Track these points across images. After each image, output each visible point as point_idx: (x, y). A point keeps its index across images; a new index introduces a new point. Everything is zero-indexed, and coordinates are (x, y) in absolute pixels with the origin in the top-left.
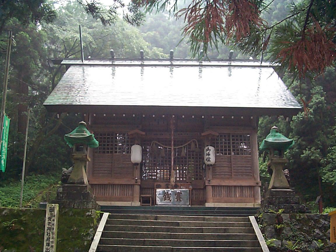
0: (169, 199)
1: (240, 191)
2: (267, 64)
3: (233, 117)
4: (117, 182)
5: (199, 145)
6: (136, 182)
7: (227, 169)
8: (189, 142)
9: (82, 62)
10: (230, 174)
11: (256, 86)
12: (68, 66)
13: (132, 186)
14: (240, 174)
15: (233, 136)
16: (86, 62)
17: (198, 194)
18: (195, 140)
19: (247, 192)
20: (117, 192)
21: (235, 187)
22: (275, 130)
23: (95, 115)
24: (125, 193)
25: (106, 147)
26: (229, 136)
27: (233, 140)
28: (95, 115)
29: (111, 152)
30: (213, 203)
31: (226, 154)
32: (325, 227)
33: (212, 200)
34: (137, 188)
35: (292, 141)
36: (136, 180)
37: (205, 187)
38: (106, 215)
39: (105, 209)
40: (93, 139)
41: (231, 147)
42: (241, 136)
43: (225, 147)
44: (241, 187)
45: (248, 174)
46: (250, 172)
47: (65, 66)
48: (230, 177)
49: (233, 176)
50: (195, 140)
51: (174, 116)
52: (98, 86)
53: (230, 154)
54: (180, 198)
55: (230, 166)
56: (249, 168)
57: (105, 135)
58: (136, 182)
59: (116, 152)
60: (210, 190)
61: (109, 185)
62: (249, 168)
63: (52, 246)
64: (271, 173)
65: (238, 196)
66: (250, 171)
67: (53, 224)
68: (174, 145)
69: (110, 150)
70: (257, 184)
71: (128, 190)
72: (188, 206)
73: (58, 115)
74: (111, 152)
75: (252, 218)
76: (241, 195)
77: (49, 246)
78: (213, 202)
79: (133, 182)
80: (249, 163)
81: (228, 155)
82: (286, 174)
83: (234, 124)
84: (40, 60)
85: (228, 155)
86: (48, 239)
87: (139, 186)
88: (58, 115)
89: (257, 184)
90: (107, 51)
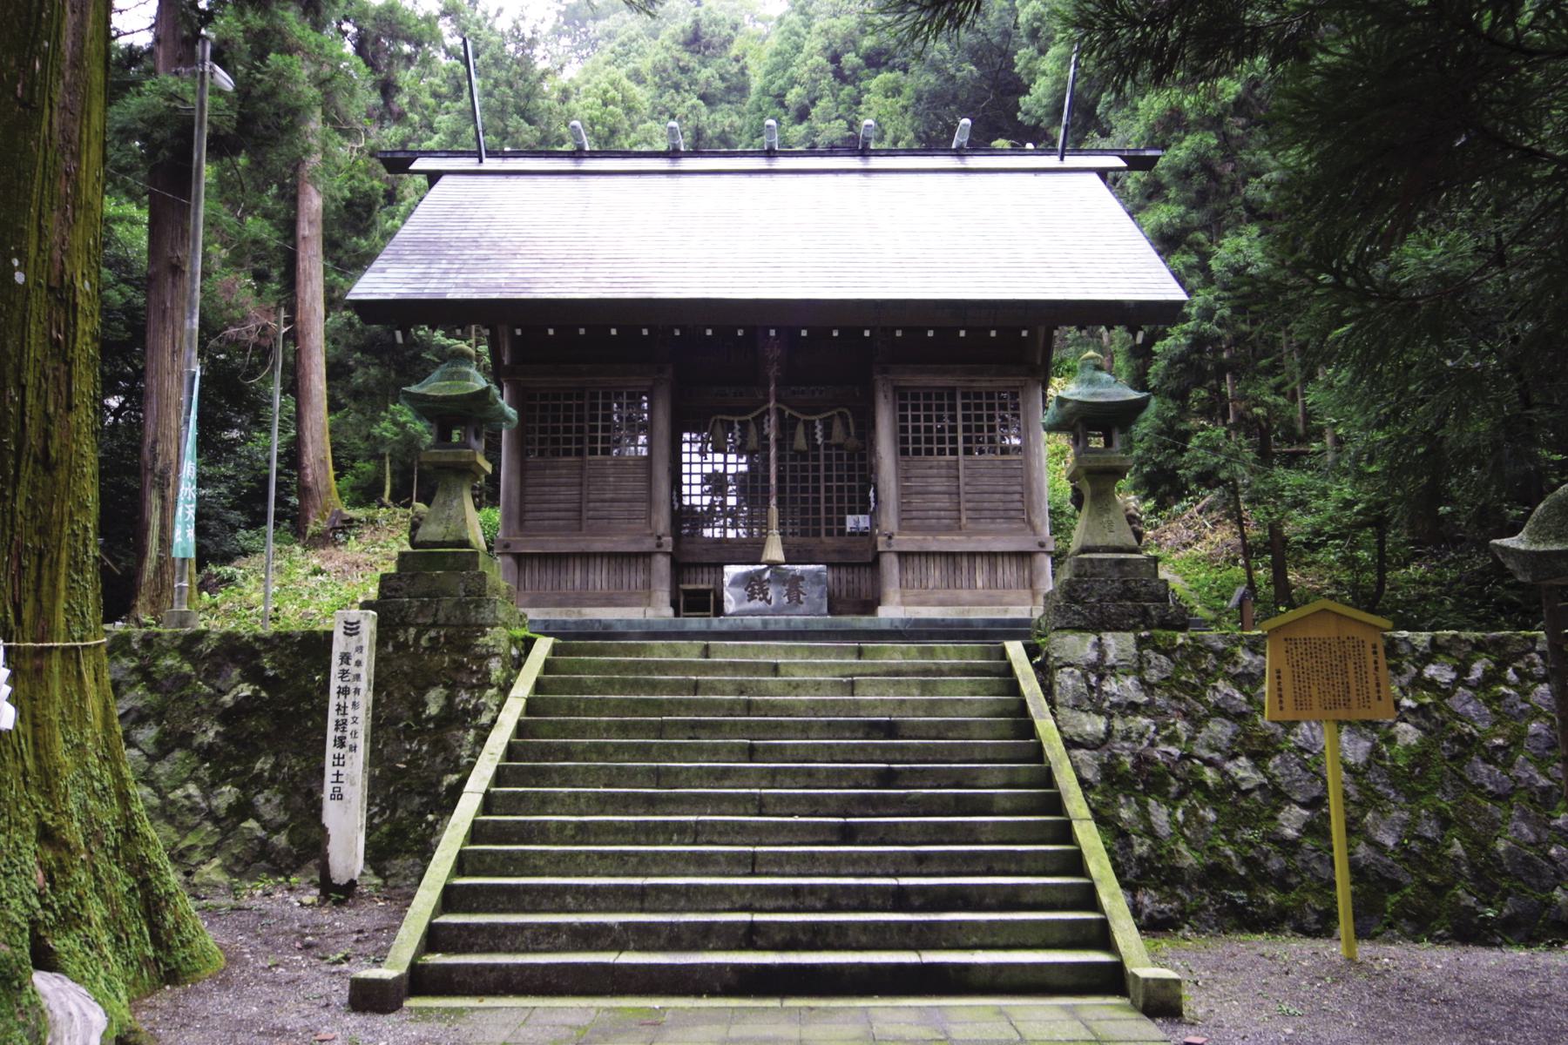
1: (986, 567)
3: (993, 333)
4: (599, 545)
5: (857, 428)
6: (659, 545)
7: (944, 501)
10: (954, 514)
11: (1052, 232)
12: (433, 177)
13: (648, 555)
14: (987, 514)
15: (965, 396)
19: (1008, 572)
20: (600, 578)
21: (972, 555)
23: (519, 332)
24: (625, 580)
25: (561, 435)
26: (952, 397)
28: (519, 332)
29: (580, 453)
31: (941, 452)
32: (1250, 675)
33: (897, 598)
34: (662, 565)
37: (877, 556)
41: (960, 430)
42: (990, 395)
44: (992, 556)
45: (1013, 513)
46: (1019, 509)
48: (955, 528)
49: (964, 521)
51: (773, 333)
52: (511, 235)
53: (954, 452)
55: (954, 489)
56: (1017, 497)
57: (568, 397)
58: (659, 545)
59: (593, 452)
60: (891, 566)
61: (574, 555)
62: (1017, 497)
63: (353, 748)
64: (1079, 506)
65: (979, 584)
66: (1019, 505)
67: (358, 677)
70: (1042, 545)
73: (399, 334)
74: (580, 453)
75: (1015, 649)
76: (992, 583)
77: (342, 745)
79: (648, 545)
80: (1013, 481)
81: (948, 457)
83: (981, 352)
84: (1173, 122)
85: (599, 457)
86: (341, 725)
88: (399, 334)
89: (1042, 545)
90: (521, 126)
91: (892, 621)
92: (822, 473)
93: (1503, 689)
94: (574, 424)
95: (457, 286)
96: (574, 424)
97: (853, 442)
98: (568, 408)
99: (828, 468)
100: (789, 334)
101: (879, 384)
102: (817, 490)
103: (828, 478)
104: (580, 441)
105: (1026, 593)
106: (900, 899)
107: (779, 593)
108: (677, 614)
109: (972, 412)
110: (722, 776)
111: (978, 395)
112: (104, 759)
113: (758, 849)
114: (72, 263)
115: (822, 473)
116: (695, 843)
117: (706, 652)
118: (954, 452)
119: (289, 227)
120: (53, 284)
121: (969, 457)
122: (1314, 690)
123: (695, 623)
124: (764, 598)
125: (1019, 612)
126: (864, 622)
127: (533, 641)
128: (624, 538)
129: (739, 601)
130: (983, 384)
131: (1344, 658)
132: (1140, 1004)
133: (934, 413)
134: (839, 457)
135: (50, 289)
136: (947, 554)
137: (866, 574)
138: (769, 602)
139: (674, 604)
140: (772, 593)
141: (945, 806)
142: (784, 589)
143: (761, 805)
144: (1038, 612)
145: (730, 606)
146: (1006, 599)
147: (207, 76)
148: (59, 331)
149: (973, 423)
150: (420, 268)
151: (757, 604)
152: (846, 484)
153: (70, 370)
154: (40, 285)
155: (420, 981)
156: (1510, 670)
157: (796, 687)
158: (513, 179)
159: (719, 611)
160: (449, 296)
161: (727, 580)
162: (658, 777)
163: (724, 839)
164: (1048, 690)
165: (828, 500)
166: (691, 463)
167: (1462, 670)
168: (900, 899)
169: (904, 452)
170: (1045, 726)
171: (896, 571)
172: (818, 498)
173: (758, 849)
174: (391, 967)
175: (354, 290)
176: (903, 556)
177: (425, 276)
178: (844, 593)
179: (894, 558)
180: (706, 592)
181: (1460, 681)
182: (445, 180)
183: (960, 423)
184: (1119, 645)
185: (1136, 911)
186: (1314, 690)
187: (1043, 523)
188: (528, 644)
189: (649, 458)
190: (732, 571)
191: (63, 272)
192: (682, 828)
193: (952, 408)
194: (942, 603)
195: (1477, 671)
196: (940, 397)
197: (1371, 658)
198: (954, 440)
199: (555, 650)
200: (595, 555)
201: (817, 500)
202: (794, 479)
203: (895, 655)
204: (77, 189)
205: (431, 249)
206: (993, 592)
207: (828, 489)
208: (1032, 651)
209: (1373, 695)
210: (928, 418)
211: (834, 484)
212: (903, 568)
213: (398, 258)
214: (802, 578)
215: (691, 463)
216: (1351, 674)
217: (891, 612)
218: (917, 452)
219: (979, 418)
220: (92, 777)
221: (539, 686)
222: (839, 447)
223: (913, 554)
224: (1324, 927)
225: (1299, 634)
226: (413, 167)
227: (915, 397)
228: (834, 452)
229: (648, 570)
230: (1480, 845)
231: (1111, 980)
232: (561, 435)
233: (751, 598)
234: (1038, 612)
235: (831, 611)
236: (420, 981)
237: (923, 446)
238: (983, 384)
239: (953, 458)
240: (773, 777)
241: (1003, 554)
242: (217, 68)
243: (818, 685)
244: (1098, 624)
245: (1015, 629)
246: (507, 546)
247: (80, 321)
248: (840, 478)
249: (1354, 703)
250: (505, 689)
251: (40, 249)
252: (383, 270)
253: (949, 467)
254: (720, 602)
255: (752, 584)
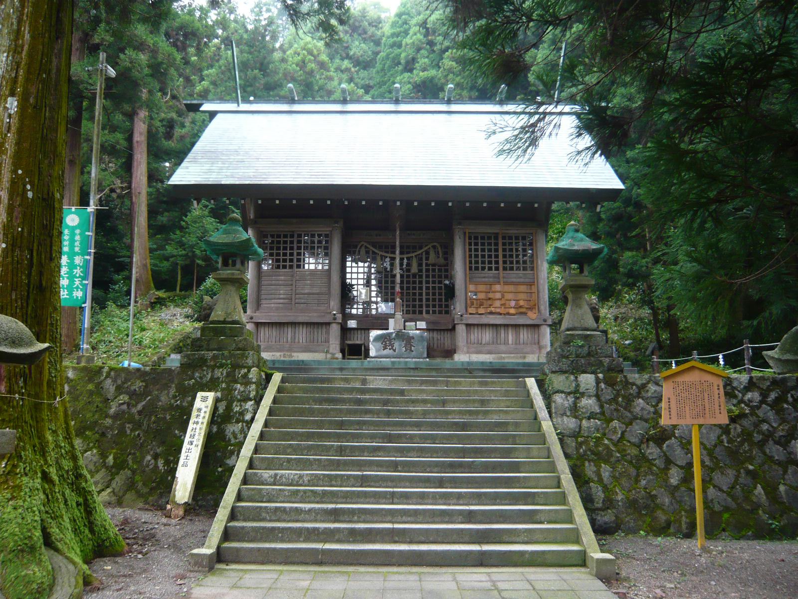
0: (392, 348)
2: (567, 109)
6: (335, 319)
8: (426, 248)
9: (238, 106)
12: (212, 114)
13: (328, 324)
15: (504, 238)
16: (244, 107)
17: (442, 339)
18: (435, 244)
19: (524, 335)
21: (506, 326)
22: (573, 227)
26: (496, 238)
27: (504, 244)
29: (291, 267)
30: (468, 355)
31: (490, 269)
34: (335, 329)
35: (603, 248)
36: (335, 315)
38: (277, 377)
39: (277, 366)
40: (253, 246)
42: (517, 238)
43: (490, 256)
47: (207, 114)
50: (435, 244)
51: (398, 203)
52: (246, 145)
53: (497, 269)
54: (412, 345)
57: (285, 236)
60: (461, 330)
66: (320, 340)
68: (401, 253)
69: (288, 264)
70: (545, 321)
71: (320, 332)
72: (425, 360)
75: (531, 382)
78: (468, 352)
81: (494, 272)
82: (594, 305)
83: (509, 219)
87: (339, 326)
89: (545, 321)
90: (261, 79)
91: (463, 363)
92: (424, 279)
93: (785, 406)
94: (288, 252)
95: (227, 176)
96: (288, 252)
97: (441, 261)
98: (285, 242)
99: (427, 276)
100: (408, 204)
101: (456, 231)
102: (421, 288)
103: (427, 282)
104: (291, 261)
105: (536, 347)
106: (470, 517)
107: (400, 345)
108: (344, 357)
109: (507, 247)
110: (375, 450)
111: (510, 238)
112: (65, 438)
113: (395, 490)
114: (53, 186)
115: (424, 279)
116: (361, 486)
117: (364, 382)
118: (497, 269)
119: (130, 139)
120: (45, 196)
121: (505, 272)
122: (687, 408)
123: (354, 363)
124: (392, 348)
125: (531, 358)
126: (447, 363)
127: (272, 375)
128: (315, 314)
129: (377, 350)
130: (513, 231)
131: (702, 392)
132: (594, 572)
133: (486, 247)
134: (434, 270)
135: (44, 199)
136: (493, 325)
137: (447, 335)
138: (395, 351)
139: (342, 351)
140: (396, 345)
141: (494, 467)
142: (403, 344)
143: (395, 466)
144: (543, 360)
145: (372, 353)
146: (525, 350)
147: (104, 72)
148: (47, 221)
149: (508, 253)
150: (207, 167)
151: (387, 352)
152: (437, 285)
153: (51, 240)
154: (39, 198)
155: (220, 557)
156: (789, 395)
157: (414, 402)
158: (256, 116)
159: (367, 355)
160: (223, 183)
161: (371, 339)
162: (341, 451)
163: (377, 484)
164: (548, 407)
165: (428, 294)
166: (351, 273)
167: (764, 395)
168: (470, 517)
169: (471, 269)
170: (547, 425)
171: (465, 334)
172: (426, 295)
173: (395, 490)
174: (209, 547)
175: (172, 179)
176: (468, 326)
177: (210, 171)
178: (436, 345)
179: (464, 327)
180: (360, 346)
181: (763, 402)
182: (219, 116)
183: (500, 253)
184: (587, 380)
185: (593, 522)
186: (687, 408)
187: (545, 309)
188: (269, 377)
189: (329, 270)
190: (374, 334)
191: (49, 190)
192: (459, 496)
193: (496, 244)
194: (490, 353)
195: (773, 396)
196: (489, 238)
197: (717, 392)
198: (497, 262)
199: (283, 380)
200: (299, 323)
201: (421, 294)
202: (408, 282)
203: (466, 384)
204: (56, 147)
205: (212, 156)
206: (518, 346)
207: (427, 288)
208: (540, 384)
209: (717, 411)
210: (483, 250)
211: (431, 285)
212: (468, 332)
213: (195, 161)
214: (413, 338)
215: (351, 273)
216: (706, 401)
217: (461, 358)
218: (477, 269)
219: (511, 244)
220: (61, 447)
221: (275, 401)
222: (434, 265)
223: (474, 325)
224: (690, 534)
225: (679, 379)
226: (201, 109)
227: (476, 238)
228: (431, 268)
229: (328, 333)
230: (771, 490)
231: (581, 560)
232: (281, 258)
233: (385, 348)
234: (543, 360)
235: (429, 356)
236: (220, 557)
237: (480, 265)
238: (513, 231)
239: (497, 272)
240: (402, 451)
241: (523, 325)
242: (109, 67)
243: (425, 402)
244: (576, 370)
245: (528, 370)
246: (252, 318)
247: (56, 215)
248: (434, 282)
249: (707, 415)
250: (258, 400)
251: (39, 180)
252: (187, 168)
253: (494, 277)
254: (367, 350)
255: (385, 340)
